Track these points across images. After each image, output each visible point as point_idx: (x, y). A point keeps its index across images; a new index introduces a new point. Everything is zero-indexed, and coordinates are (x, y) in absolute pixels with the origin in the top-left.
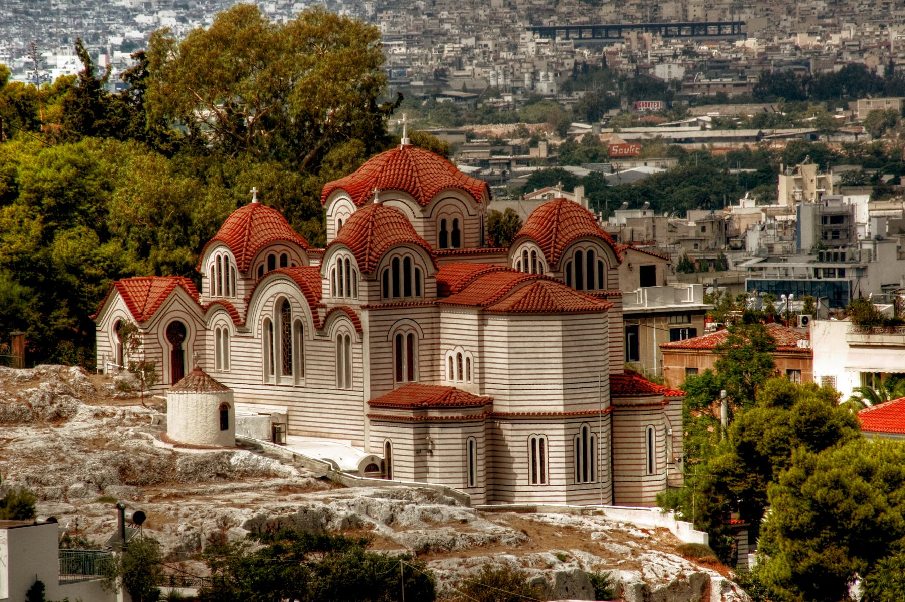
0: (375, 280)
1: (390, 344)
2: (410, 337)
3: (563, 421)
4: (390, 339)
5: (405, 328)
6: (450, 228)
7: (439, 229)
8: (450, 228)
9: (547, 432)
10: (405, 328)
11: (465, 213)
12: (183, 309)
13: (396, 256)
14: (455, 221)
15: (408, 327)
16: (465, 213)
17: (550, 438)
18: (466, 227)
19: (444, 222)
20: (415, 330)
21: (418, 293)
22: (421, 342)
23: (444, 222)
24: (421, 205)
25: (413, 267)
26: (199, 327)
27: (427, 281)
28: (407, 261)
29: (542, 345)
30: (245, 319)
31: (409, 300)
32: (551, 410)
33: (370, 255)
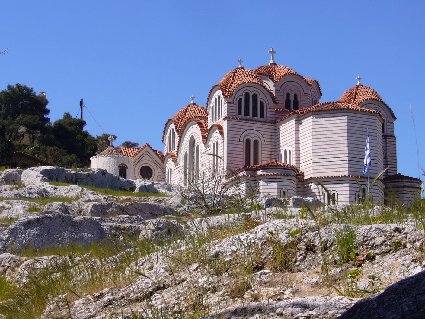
0: (233, 103)
1: (242, 143)
2: (256, 142)
3: (348, 181)
4: (241, 140)
5: (253, 135)
6: (292, 99)
7: (285, 98)
8: (292, 99)
9: (336, 189)
10: (253, 135)
11: (302, 91)
12: (150, 160)
13: (248, 91)
14: (296, 96)
15: (255, 135)
16: (302, 91)
17: (339, 193)
18: (302, 99)
19: (288, 95)
20: (260, 138)
21: (262, 116)
22: (263, 146)
23: (288, 95)
24: (274, 82)
25: (259, 101)
26: (160, 171)
27: (268, 110)
28: (255, 96)
29: (334, 132)
30: (177, 154)
31: (255, 118)
32: (340, 174)
33: (230, 88)
